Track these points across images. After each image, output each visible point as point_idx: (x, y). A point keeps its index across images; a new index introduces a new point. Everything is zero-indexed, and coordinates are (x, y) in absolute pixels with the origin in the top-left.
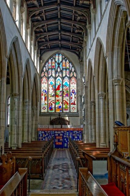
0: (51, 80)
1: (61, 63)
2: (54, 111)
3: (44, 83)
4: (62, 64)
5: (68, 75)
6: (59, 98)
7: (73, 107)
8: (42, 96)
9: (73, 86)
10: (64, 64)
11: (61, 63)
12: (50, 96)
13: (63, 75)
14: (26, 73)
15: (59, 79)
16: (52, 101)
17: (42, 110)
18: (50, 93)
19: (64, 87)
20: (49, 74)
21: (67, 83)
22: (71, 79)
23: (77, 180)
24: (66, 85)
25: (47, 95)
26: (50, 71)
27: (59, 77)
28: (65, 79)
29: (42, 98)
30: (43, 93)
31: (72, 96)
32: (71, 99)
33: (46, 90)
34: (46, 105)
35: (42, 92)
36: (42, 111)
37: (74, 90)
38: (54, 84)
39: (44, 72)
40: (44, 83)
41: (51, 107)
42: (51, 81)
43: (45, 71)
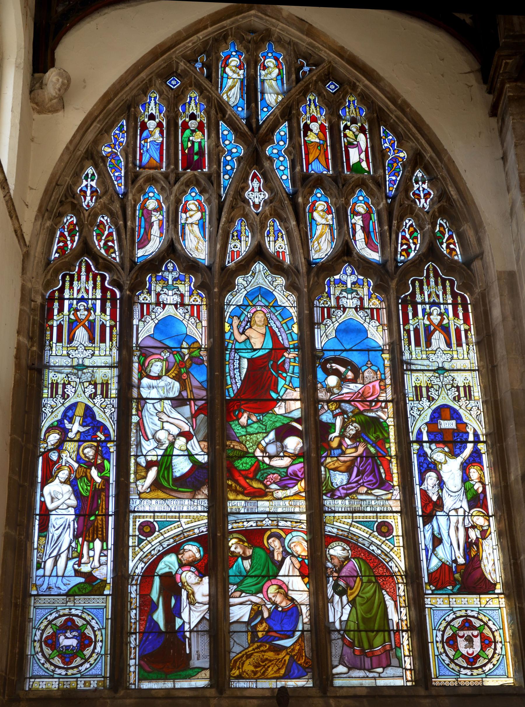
0: (170, 298)
1: (284, 129)
2: (200, 682)
3: (81, 334)
4: (293, 134)
5: (369, 243)
6: (263, 505)
7: (467, 625)
8: (48, 478)
9: (441, 370)
10: (312, 138)
11: (284, 129)
12: (156, 485)
13: (314, 245)
14: (89, 130)
15: (267, 294)
16: (176, 549)
17: (34, 669)
18: (148, 446)
19: (332, 381)
20: (145, 241)
21: (362, 332)
22: (402, 286)
23: (171, 497)
24: (356, 358)
25: (111, 467)
26: (152, 204)
27: (259, 266)
28: (335, 291)
29: (45, 514)
30: (59, 447)
31: (431, 478)
32: (428, 518)
33: (100, 416)
34: (96, 601)
35: (54, 438)
36: (41, 684)
37: (455, 415)
38: (202, 340)
39: (77, 209)
40: (81, 334)
41: (159, 616)
42: (161, 314)
43: (88, 201)
